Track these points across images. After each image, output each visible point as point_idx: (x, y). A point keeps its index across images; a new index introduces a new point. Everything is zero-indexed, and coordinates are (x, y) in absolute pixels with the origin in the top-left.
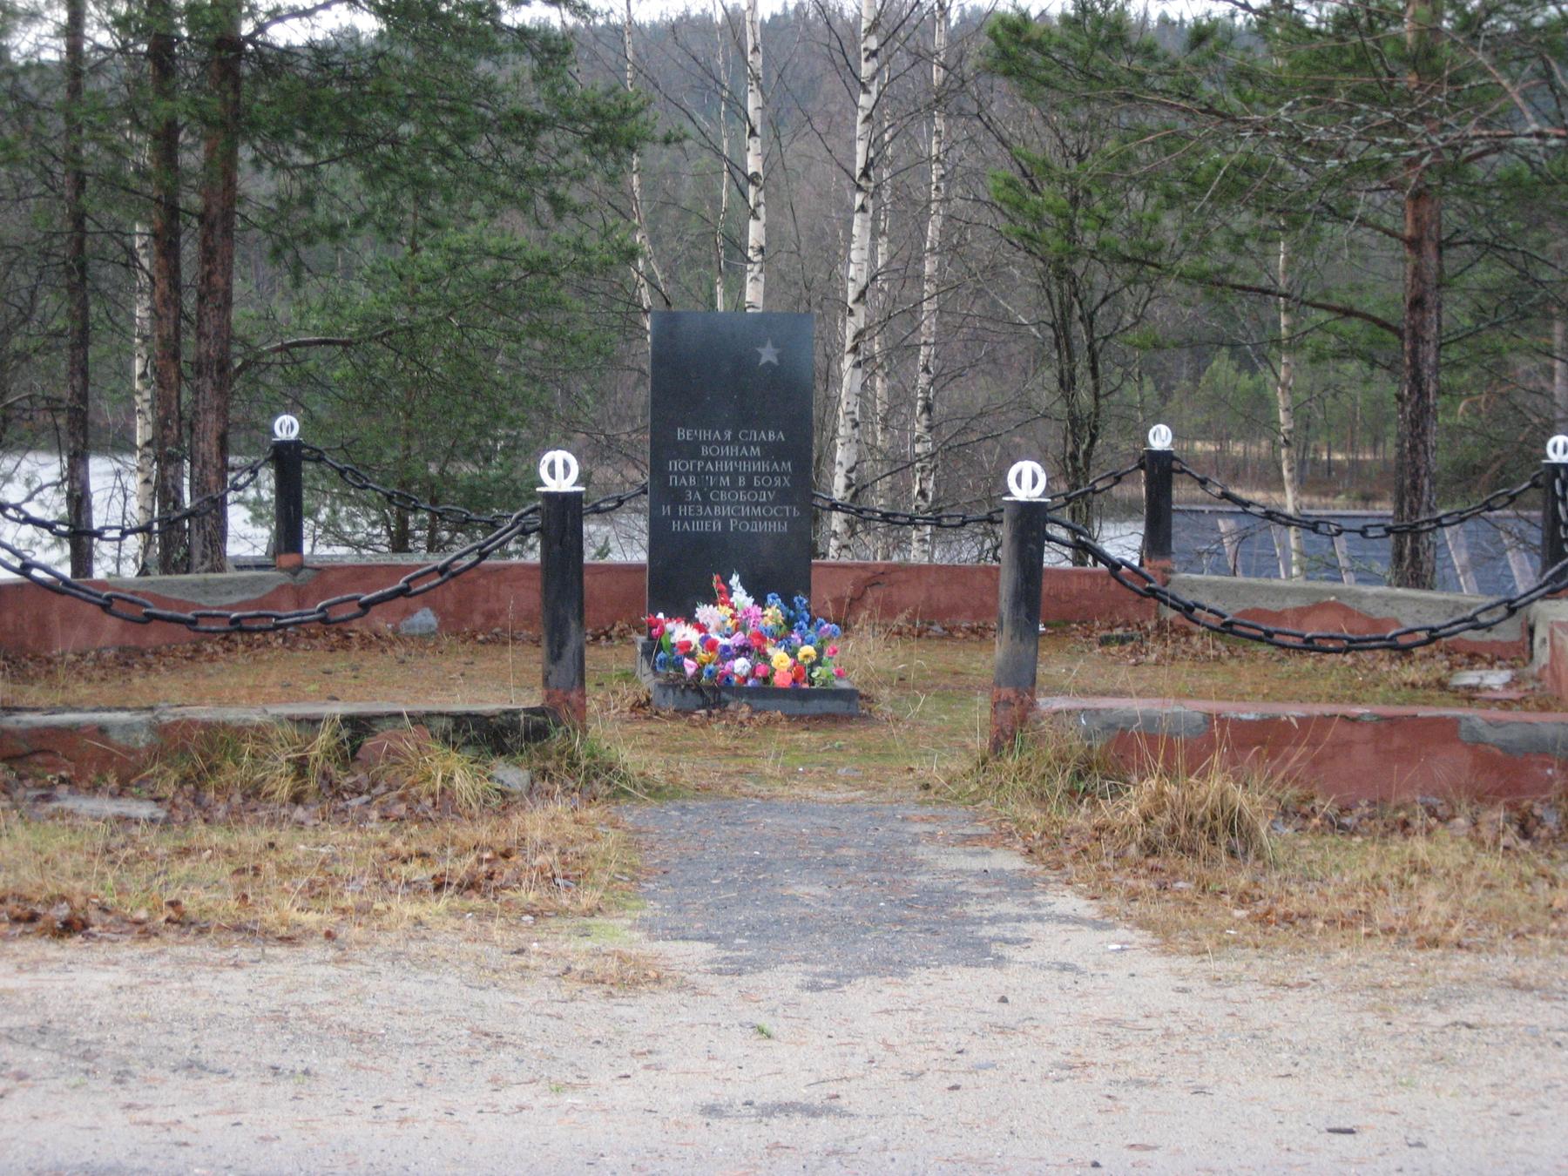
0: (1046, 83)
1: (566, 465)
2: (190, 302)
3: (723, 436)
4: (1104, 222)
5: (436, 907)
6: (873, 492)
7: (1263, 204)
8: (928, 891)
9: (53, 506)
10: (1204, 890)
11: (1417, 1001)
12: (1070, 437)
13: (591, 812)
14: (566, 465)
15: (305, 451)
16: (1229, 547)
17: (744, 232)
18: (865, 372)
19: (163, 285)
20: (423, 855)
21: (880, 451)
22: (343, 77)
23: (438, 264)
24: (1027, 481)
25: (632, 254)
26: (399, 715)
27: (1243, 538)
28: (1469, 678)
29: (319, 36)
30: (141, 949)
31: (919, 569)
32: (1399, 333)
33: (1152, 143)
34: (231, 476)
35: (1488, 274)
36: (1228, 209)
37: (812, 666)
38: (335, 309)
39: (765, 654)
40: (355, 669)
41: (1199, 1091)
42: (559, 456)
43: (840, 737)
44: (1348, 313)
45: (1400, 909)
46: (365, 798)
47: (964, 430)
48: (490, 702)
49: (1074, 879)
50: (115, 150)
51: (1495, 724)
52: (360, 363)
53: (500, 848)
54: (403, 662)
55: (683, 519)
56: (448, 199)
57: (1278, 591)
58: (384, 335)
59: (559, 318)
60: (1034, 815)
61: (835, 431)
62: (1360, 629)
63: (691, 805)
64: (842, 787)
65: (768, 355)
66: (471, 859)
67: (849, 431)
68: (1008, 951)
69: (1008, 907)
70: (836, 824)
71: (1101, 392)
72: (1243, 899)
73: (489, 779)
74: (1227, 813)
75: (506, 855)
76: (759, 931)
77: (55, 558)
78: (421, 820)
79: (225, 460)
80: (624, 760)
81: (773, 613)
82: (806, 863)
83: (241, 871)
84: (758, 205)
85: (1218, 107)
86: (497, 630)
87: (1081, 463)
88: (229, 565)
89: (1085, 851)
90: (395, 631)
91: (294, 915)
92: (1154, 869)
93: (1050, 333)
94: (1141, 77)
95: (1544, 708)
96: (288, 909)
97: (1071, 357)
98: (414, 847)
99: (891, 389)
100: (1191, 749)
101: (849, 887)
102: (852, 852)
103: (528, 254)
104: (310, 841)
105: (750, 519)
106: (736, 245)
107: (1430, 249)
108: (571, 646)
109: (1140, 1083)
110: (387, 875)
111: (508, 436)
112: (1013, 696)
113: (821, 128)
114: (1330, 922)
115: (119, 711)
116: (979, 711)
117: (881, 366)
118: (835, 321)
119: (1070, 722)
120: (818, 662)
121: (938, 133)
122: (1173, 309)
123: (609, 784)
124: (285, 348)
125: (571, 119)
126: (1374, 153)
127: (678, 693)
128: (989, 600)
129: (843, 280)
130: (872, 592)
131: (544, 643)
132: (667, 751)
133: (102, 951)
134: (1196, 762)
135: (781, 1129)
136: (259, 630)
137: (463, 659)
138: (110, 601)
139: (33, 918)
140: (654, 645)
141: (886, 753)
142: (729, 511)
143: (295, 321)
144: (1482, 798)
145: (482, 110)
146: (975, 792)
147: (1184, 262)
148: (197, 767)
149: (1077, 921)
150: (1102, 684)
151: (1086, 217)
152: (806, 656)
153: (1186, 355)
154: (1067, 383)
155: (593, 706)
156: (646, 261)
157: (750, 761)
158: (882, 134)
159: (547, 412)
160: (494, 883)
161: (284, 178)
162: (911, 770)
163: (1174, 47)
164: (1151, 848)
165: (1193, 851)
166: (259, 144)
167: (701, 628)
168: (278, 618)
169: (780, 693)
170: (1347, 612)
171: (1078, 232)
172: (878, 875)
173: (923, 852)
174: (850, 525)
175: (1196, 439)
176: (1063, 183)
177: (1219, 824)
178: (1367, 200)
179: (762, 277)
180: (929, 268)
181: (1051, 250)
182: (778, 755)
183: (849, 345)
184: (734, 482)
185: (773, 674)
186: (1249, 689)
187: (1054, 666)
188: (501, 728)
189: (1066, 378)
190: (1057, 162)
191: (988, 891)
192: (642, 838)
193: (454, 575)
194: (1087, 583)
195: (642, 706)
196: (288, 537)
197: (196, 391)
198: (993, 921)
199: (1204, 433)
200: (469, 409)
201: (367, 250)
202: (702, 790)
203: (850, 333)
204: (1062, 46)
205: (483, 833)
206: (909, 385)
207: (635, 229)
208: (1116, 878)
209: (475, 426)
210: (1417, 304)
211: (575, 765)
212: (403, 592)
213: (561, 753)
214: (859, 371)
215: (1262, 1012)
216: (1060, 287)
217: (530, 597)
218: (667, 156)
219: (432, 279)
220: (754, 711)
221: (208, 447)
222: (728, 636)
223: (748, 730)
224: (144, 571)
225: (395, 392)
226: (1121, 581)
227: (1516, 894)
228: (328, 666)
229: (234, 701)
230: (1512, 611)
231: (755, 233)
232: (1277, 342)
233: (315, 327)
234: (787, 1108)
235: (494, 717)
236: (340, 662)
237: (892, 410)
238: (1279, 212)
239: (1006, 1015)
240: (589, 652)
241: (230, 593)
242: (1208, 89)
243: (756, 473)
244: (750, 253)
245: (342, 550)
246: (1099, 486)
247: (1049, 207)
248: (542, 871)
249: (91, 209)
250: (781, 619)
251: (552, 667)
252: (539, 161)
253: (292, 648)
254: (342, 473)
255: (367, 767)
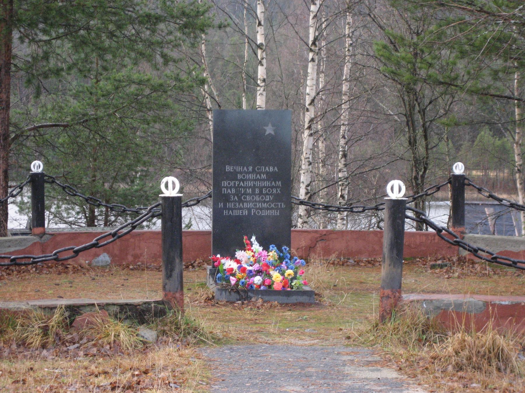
1: (173, 183)
3: (248, 169)
4: (430, 65)
6: (318, 196)
10: (486, 388)
12: (414, 169)
13: (187, 351)
14: (173, 183)
15: (46, 178)
16: (490, 222)
17: (256, 72)
18: (314, 139)
20: (106, 373)
21: (322, 176)
23: (109, 87)
24: (396, 190)
25: (203, 82)
26: (93, 305)
33: (454, 26)
34: (10, 190)
36: (490, 58)
37: (292, 279)
39: (269, 274)
40: (71, 283)
42: (170, 179)
43: (306, 314)
46: (77, 345)
48: (137, 298)
49: (422, 382)
52: (72, 135)
53: (143, 369)
54: (94, 279)
55: (229, 209)
56: (114, 56)
57: (516, 242)
58: (84, 122)
59: (167, 113)
60: (402, 351)
61: (300, 167)
63: (235, 347)
64: (308, 338)
65: (269, 130)
66: (129, 375)
67: (307, 167)
70: (305, 356)
71: (429, 147)
73: (137, 335)
74: (496, 350)
75: (146, 372)
78: (105, 356)
79: (7, 183)
80: (202, 325)
81: (273, 254)
82: (291, 375)
83: (17, 382)
84: (263, 59)
85: (485, 9)
86: (139, 263)
87: (419, 181)
88: (9, 233)
89: (427, 369)
90: (89, 264)
92: (461, 378)
93: (404, 119)
97: (414, 130)
98: (101, 369)
99: (326, 147)
100: (478, 319)
101: (313, 387)
102: (313, 370)
103: (152, 82)
105: (261, 209)
106: (252, 78)
110: (88, 383)
111: (142, 171)
112: (390, 293)
113: (293, 21)
116: (374, 301)
117: (322, 135)
118: (299, 114)
119: (418, 306)
120: (295, 278)
121: (349, 24)
122: (463, 107)
123: (195, 337)
124: (36, 128)
125: (173, 17)
127: (228, 293)
128: (377, 248)
129: (304, 94)
130: (320, 244)
131: (163, 269)
132: (223, 321)
134: (480, 326)
136: (25, 265)
137: (123, 277)
140: (215, 270)
142: (251, 205)
143: (40, 115)
145: (130, 13)
146: (373, 340)
147: (469, 84)
150: (434, 287)
151: (421, 63)
152: (289, 275)
153: (467, 129)
154: (412, 143)
155: (187, 300)
156: (209, 86)
157: (263, 326)
158: (321, 25)
159: (161, 159)
160: (140, 386)
161: (34, 47)
162: (341, 329)
164: (459, 367)
165: (479, 369)
166: (22, 30)
167: (238, 262)
168: (34, 258)
169: (277, 293)
171: (418, 70)
172: (326, 381)
173: (348, 370)
175: (474, 169)
176: (410, 46)
177: (492, 355)
179: (264, 93)
180: (345, 88)
181: (404, 78)
182: (276, 323)
183: (306, 125)
184: (254, 191)
185: (273, 284)
186: (504, 290)
187: (409, 279)
188: (143, 311)
189: (412, 141)
190: (408, 37)
191: (379, 388)
192: (211, 363)
193: (119, 237)
194: (424, 238)
195: (210, 300)
196: (38, 219)
199: (477, 166)
200: (125, 157)
201: (73, 81)
203: (307, 120)
206: (336, 144)
207: (204, 70)
208: (443, 382)
209: (126, 166)
211: (179, 328)
213: (171, 323)
214: (312, 138)
216: (409, 96)
217: (156, 247)
220: (264, 302)
222: (251, 266)
223: (261, 311)
225: (89, 149)
226: (443, 238)
228: (57, 282)
229: (12, 299)
231: (261, 72)
232: (515, 122)
233: (50, 118)
235: (139, 305)
236: (63, 279)
237: (328, 155)
238: (515, 59)
240: (185, 273)
241: (9, 246)
243: (264, 187)
244: (259, 82)
245: (63, 226)
246: (429, 192)
247: (403, 59)
248: (163, 380)
250: (276, 257)
251: (167, 281)
252: (157, 38)
253: (40, 273)
254: (64, 188)
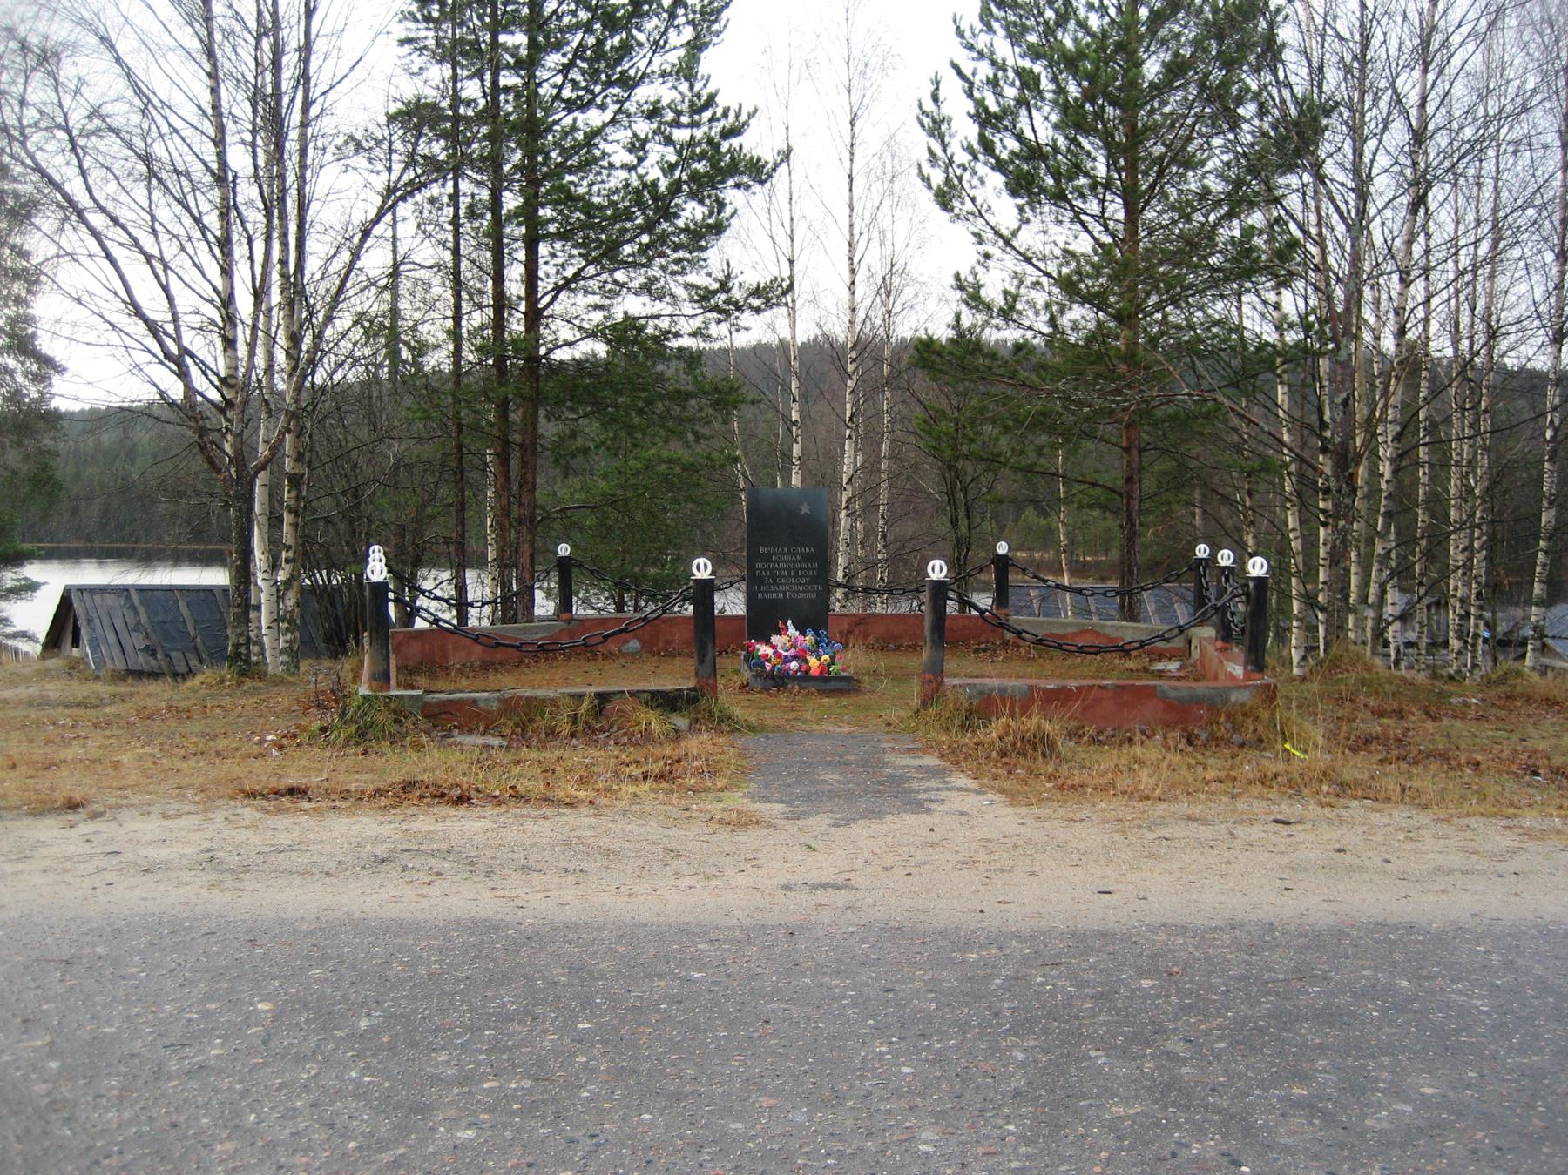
0: (942, 372)
2: (515, 487)
4: (972, 441)
5: (645, 787)
7: (1051, 430)
8: (892, 777)
9: (448, 591)
11: (1140, 827)
19: (501, 480)
20: (637, 762)
22: (590, 375)
24: (937, 570)
27: (1043, 599)
28: (1160, 666)
29: (578, 356)
30: (497, 810)
31: (881, 616)
32: (1120, 495)
35: (1166, 465)
37: (829, 666)
38: (585, 489)
41: (1033, 874)
42: (702, 561)
43: (844, 701)
44: (1094, 485)
45: (1129, 781)
47: (903, 547)
50: (478, 412)
51: (1175, 689)
56: (644, 434)
62: (1103, 643)
65: (805, 509)
66: (661, 763)
68: (933, 806)
69: (933, 784)
72: (1050, 778)
75: (679, 761)
76: (807, 798)
77: (450, 616)
78: (634, 745)
81: (810, 638)
82: (830, 763)
91: (573, 792)
94: (990, 368)
95: (1197, 680)
96: (570, 790)
100: (1023, 703)
104: (580, 755)
106: (787, 456)
107: (1135, 453)
108: (709, 658)
109: (1002, 871)
114: (1095, 789)
115: (483, 693)
116: (915, 688)
122: (1007, 484)
124: (562, 510)
126: (1107, 404)
129: (842, 472)
130: (860, 624)
133: (478, 811)
135: (821, 896)
138: (477, 637)
139: (443, 795)
140: (750, 655)
141: (868, 708)
144: (1168, 726)
148: (522, 721)
149: (967, 790)
154: (954, 522)
155: (720, 687)
159: (693, 541)
163: (1005, 354)
165: (1025, 755)
167: (774, 647)
170: (1098, 634)
173: (888, 757)
174: (846, 595)
178: (1102, 429)
187: (951, 664)
196: (565, 605)
197: (518, 532)
198: (925, 791)
201: (602, 462)
202: (776, 728)
203: (844, 500)
204: (950, 353)
205: (668, 751)
210: (1129, 480)
212: (625, 630)
215: (1062, 834)
217: (688, 632)
218: (753, 409)
219: (637, 473)
221: (525, 560)
224: (493, 623)
227: (1186, 773)
229: (540, 687)
230: (1181, 632)
231: (796, 450)
234: (825, 886)
236: (592, 667)
237: (866, 537)
239: (934, 838)
242: (1023, 374)
245: (591, 612)
249: (466, 441)
253: (569, 660)
255: (607, 718)
